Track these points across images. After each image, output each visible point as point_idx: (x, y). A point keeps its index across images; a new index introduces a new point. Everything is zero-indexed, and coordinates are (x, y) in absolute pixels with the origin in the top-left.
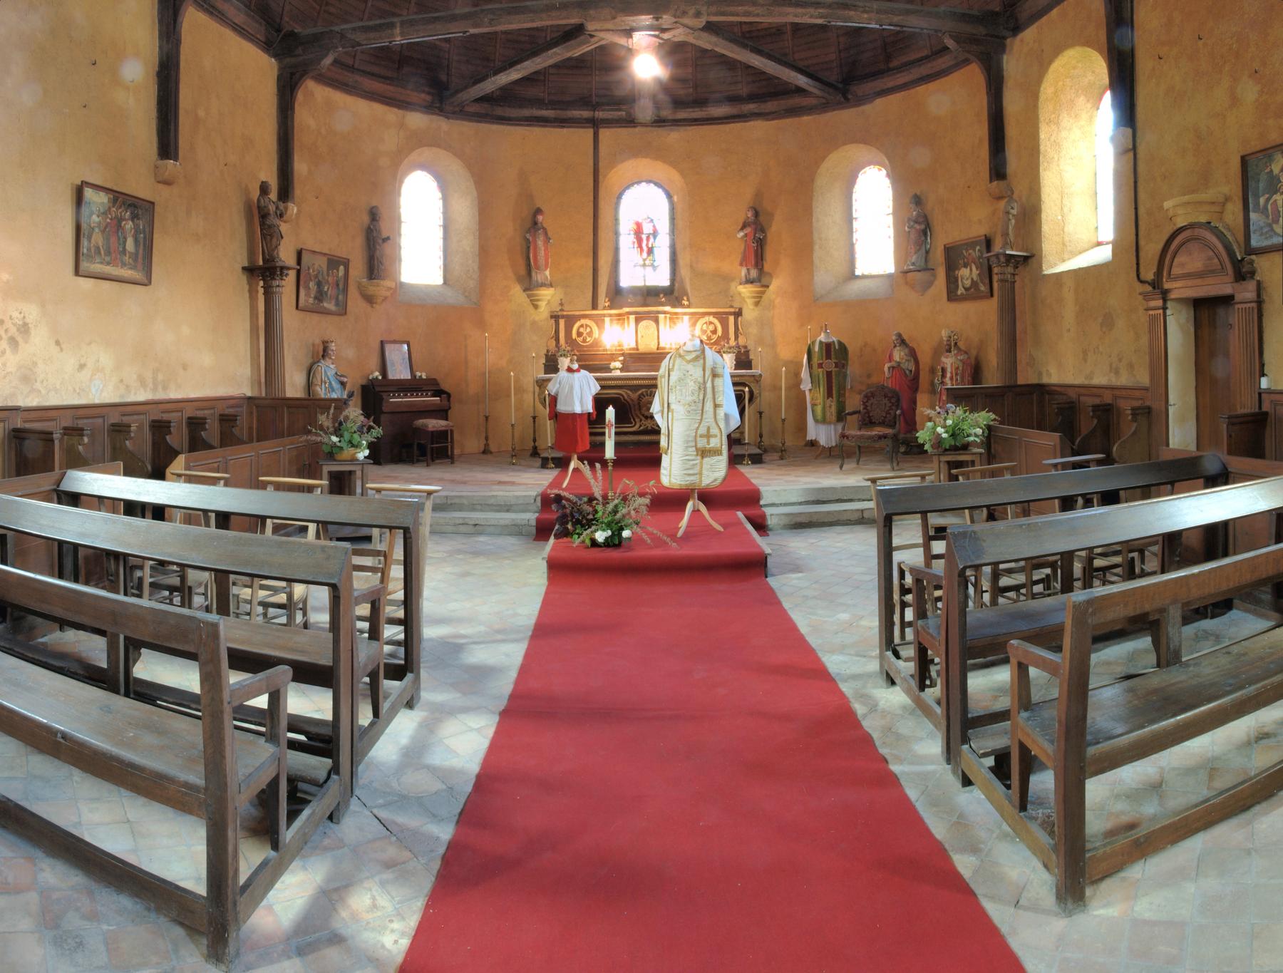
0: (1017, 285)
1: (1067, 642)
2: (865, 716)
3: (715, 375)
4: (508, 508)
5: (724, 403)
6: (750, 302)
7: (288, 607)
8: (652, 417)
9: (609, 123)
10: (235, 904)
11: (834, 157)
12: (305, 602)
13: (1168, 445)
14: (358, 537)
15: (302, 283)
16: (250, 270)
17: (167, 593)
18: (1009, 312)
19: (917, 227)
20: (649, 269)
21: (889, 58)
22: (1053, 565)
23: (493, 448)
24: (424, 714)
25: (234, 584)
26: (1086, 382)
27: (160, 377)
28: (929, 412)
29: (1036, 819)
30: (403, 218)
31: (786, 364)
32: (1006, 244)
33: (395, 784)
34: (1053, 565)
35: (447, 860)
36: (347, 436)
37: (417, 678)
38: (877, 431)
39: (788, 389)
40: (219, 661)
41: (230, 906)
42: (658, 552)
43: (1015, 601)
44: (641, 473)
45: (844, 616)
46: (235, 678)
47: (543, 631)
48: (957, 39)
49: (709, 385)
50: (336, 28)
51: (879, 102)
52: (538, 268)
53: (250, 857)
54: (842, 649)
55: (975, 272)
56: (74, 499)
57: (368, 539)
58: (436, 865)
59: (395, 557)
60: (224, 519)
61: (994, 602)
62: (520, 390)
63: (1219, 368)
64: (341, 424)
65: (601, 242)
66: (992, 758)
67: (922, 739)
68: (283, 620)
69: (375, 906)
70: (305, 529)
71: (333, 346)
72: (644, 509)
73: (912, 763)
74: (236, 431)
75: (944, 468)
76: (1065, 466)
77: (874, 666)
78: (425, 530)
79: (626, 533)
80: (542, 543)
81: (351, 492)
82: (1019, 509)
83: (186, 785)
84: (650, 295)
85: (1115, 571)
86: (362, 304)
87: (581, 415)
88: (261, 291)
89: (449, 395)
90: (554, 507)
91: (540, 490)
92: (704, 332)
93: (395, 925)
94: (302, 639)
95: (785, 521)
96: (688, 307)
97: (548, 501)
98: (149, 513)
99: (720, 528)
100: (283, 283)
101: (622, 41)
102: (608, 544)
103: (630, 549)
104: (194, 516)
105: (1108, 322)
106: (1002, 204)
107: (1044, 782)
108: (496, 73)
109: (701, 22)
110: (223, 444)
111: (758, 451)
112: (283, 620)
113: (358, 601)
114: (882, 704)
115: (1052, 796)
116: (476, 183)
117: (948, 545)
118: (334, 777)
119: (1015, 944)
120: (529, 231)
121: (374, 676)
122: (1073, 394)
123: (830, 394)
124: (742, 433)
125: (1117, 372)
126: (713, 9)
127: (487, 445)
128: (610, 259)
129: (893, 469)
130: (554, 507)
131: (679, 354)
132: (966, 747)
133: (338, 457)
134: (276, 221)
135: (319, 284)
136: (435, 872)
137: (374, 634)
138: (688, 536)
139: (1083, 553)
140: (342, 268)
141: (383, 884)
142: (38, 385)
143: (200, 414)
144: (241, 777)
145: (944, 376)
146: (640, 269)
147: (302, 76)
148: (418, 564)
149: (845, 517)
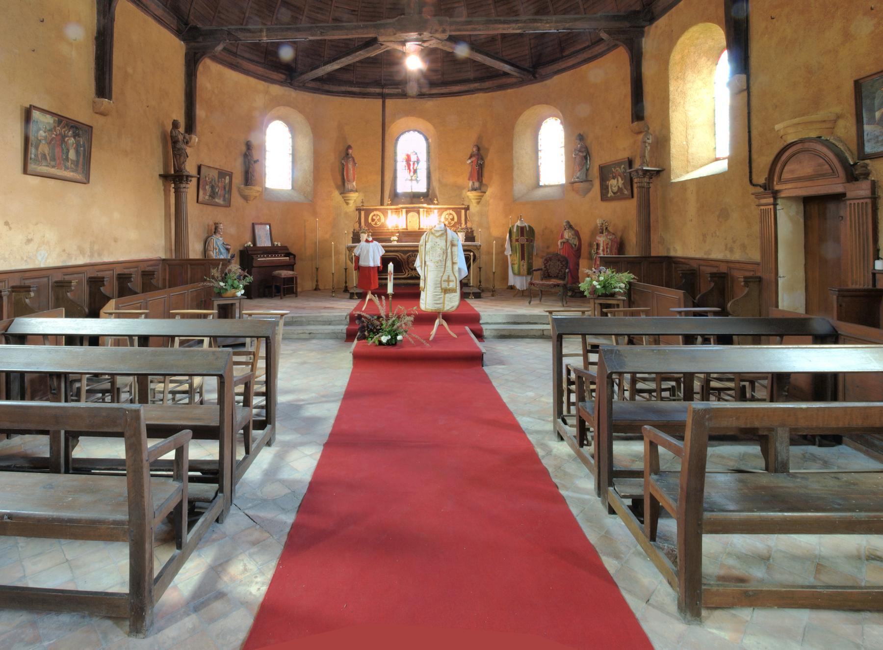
0: (651, 190)
1: (688, 434)
2: (544, 457)
3: (453, 245)
4: (330, 323)
5: (458, 261)
6: (474, 201)
7: (190, 392)
8: (415, 269)
9: (391, 96)
10: (150, 592)
11: (527, 113)
12: (201, 388)
13: (777, 306)
14: (237, 344)
15: (201, 186)
16: (165, 177)
17: (100, 395)
18: (645, 208)
19: (581, 154)
20: (414, 182)
21: (563, 50)
22: (677, 380)
23: (321, 287)
24: (277, 448)
25: (151, 382)
26: (705, 257)
27: (96, 247)
29: (663, 549)
30: (267, 149)
31: (496, 239)
32: (643, 164)
33: (259, 494)
34: (677, 380)
35: (291, 535)
36: (230, 282)
40: (140, 434)
41: (146, 594)
42: (418, 349)
43: (648, 400)
44: (409, 302)
45: (531, 394)
46: (151, 443)
47: (350, 395)
48: (609, 33)
49: (449, 251)
50: (225, 28)
51: (556, 78)
53: (161, 557)
54: (529, 414)
55: (621, 182)
56: (22, 339)
57: (243, 345)
58: (284, 539)
59: (260, 355)
60: (144, 340)
61: (632, 398)
62: (337, 253)
64: (226, 274)
65: (386, 166)
66: (630, 500)
67: (581, 477)
68: (187, 401)
69: (245, 570)
70: (202, 341)
71: (221, 226)
72: (410, 323)
73: (574, 492)
74: (154, 282)
75: (598, 307)
76: (687, 313)
77: (550, 427)
78: (279, 337)
79: (399, 338)
80: (349, 343)
81: (233, 317)
82: (651, 339)
83: (115, 522)
84: (415, 197)
85: (729, 392)
86: (241, 201)
87: (373, 268)
88: (173, 190)
89: (295, 256)
90: (357, 322)
91: (349, 312)
92: (446, 219)
93: (259, 579)
94: (199, 411)
95: (494, 333)
97: (353, 318)
98: (86, 342)
99: (455, 336)
100: (188, 186)
101: (400, 48)
102: (389, 343)
103: (401, 347)
104: (120, 340)
105: (724, 214)
106: (641, 136)
107: (669, 526)
108: (325, 64)
109: (445, 36)
111: (478, 291)
112: (187, 401)
113: (236, 384)
114: (555, 451)
115: (675, 537)
116: (312, 129)
117: (600, 357)
118: (220, 495)
119: (646, 627)
120: (343, 159)
121: (246, 429)
122: (694, 265)
123: (523, 258)
125: (731, 250)
126: (453, 27)
127: (317, 285)
128: (391, 176)
130: (357, 322)
131: (432, 232)
132: (611, 489)
133: (224, 295)
134: (184, 146)
135: (212, 187)
136: (283, 543)
137: (247, 403)
138: (436, 340)
139: (702, 376)
140: (228, 177)
141: (251, 555)
143: (126, 271)
144: (155, 507)
145: (598, 248)
147: (202, 55)
148: (275, 364)
149: (532, 334)
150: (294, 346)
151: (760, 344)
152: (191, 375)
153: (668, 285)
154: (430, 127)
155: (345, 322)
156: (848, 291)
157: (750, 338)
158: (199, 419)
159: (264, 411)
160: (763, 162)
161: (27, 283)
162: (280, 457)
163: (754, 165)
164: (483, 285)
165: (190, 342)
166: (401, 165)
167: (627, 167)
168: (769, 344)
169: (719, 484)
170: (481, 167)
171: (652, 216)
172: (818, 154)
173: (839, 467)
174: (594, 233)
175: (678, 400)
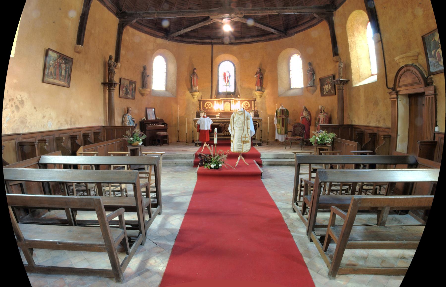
0: (344, 91)
2: (286, 219)
3: (247, 119)
4: (185, 158)
5: (250, 127)
6: (258, 97)
7: (121, 191)
8: (228, 131)
12: (126, 189)
13: (396, 150)
14: (140, 169)
16: (104, 84)
17: (82, 192)
18: (341, 100)
19: (310, 72)
20: (228, 87)
22: (350, 186)
23: (180, 140)
26: (368, 125)
27: (73, 120)
28: (314, 132)
31: (269, 116)
32: (340, 77)
34: (350, 186)
36: (135, 138)
37: (161, 206)
38: (297, 137)
39: (270, 123)
42: (229, 171)
43: (336, 195)
45: (283, 192)
46: (108, 214)
47: (196, 192)
48: (318, 14)
49: (246, 122)
50: (138, 12)
51: (296, 35)
52: (194, 86)
54: (281, 201)
56: (45, 166)
57: (144, 169)
60: (97, 167)
61: (329, 194)
62: (189, 123)
63: (419, 122)
64: (133, 134)
68: (120, 195)
70: (124, 167)
71: (130, 109)
74: (99, 137)
76: (358, 153)
77: (290, 206)
78: (161, 165)
79: (220, 165)
80: (195, 168)
81: (138, 155)
82: (341, 166)
84: (228, 94)
85: (370, 191)
87: (207, 130)
88: (107, 91)
89: (167, 124)
90: (199, 158)
91: (195, 153)
92: (244, 106)
94: (126, 199)
95: (268, 163)
96: (240, 98)
97: (197, 156)
98: (72, 167)
99: (248, 164)
101: (220, 21)
102: (215, 168)
103: (221, 169)
104: (87, 166)
105: (376, 103)
106: (338, 64)
109: (242, 16)
110: (95, 142)
111: (260, 142)
112: (120, 195)
113: (142, 187)
114: (291, 217)
120: (192, 75)
121: (148, 207)
122: (363, 129)
123: (283, 125)
124: (256, 137)
125: (379, 122)
128: (216, 83)
129: (302, 150)
130: (199, 158)
131: (237, 112)
132: (313, 232)
133: (133, 144)
134: (114, 68)
135: (126, 89)
137: (147, 196)
138: (238, 166)
139: (360, 183)
140: (134, 84)
142: (27, 125)
143: (87, 132)
146: (225, 87)
150: (168, 169)
151: (386, 168)
152: (120, 183)
153: (351, 140)
154: (236, 59)
155: (193, 158)
156: (424, 142)
157: (383, 165)
158: (127, 203)
159: (156, 199)
160: (391, 76)
161: (45, 138)
162: (165, 219)
163: (388, 78)
164: (263, 139)
165: (119, 167)
166: (221, 78)
167: (333, 79)
168: (390, 168)
169: (358, 230)
170: (262, 79)
171: (344, 104)
172: (413, 73)
173: (404, 224)
174: (317, 113)
175: (349, 195)
